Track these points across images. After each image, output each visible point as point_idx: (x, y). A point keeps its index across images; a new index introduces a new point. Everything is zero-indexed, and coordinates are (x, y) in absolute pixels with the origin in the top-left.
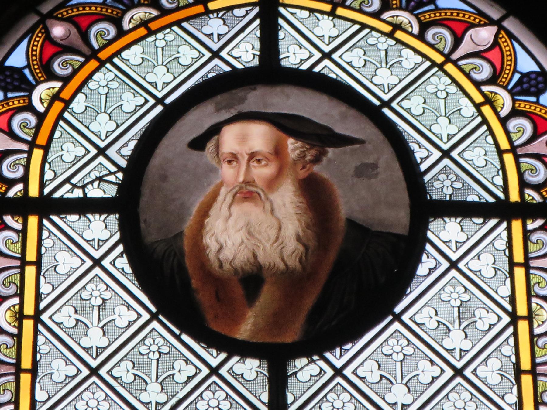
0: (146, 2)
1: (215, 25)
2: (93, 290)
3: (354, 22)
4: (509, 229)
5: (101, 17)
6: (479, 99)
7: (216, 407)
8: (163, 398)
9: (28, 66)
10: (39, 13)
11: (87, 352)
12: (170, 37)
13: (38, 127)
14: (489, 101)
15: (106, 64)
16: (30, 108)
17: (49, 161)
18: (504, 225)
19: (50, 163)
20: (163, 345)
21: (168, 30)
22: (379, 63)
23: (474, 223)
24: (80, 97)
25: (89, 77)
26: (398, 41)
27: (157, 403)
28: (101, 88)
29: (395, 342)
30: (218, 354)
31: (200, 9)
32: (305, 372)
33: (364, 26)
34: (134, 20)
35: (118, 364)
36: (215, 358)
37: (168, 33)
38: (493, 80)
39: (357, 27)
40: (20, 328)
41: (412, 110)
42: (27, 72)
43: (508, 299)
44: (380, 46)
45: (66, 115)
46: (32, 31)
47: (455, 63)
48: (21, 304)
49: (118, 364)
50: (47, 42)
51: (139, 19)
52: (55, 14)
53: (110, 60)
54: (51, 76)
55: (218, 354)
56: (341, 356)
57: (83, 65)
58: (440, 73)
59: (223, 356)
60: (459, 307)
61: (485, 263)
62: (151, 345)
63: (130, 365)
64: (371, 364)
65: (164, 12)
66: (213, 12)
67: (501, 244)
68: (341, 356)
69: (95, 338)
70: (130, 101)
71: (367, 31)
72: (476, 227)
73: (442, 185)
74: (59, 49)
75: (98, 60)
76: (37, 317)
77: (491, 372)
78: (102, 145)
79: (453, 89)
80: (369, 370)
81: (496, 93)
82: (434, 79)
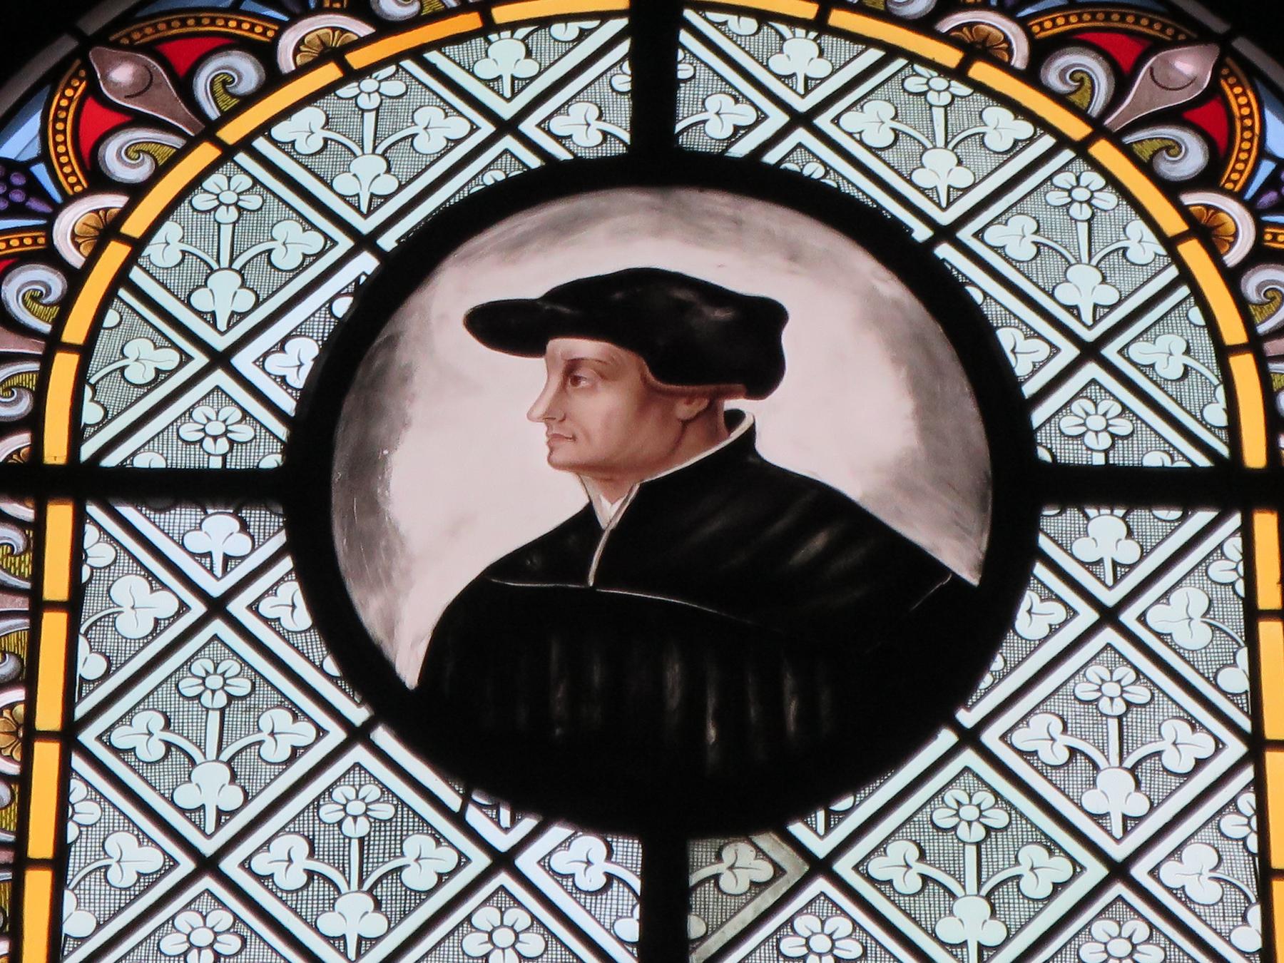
0: (337, 5)
1: (505, 56)
2: (207, 673)
3: (870, 42)
4: (1246, 532)
5: (226, 41)
6: (1173, 224)
7: (1125, 958)
8: (994, 934)
9: (44, 157)
10: (78, 34)
11: (1098, 824)
12: (395, 88)
13: (66, 304)
14: (1205, 231)
15: (236, 154)
16: (50, 257)
17: (93, 381)
18: (1235, 520)
19: (94, 387)
20: (377, 801)
21: (392, 69)
22: (934, 141)
23: (1155, 517)
24: (170, 229)
25: (196, 183)
26: (979, 87)
27: (981, 947)
28: (223, 208)
29: (351, 793)
30: (514, 821)
31: (471, 21)
32: (735, 868)
33: (892, 52)
34: (971, 32)
35: (880, 849)
36: (821, 837)
37: (386, 79)
38: (1208, 179)
39: (874, 55)
40: (27, 762)
41: (1007, 250)
42: (40, 171)
43: (1243, 700)
44: (932, 97)
45: (136, 275)
46: (53, 79)
47: (1115, 139)
48: (30, 703)
49: (880, 849)
50: (90, 104)
51: (318, 42)
52: (113, 38)
53: (245, 145)
54: (100, 181)
55: (514, 821)
56: (828, 828)
57: (179, 155)
58: (1080, 165)
59: (528, 824)
60: (222, 710)
61: (1183, 617)
62: (348, 801)
63: (301, 847)
64: (903, 849)
65: (386, 27)
66: (499, 28)
67: (1226, 570)
68: (828, 828)
69: (210, 787)
70: (293, 242)
71: (901, 62)
72: (1169, 527)
73: (1077, 428)
74: (127, 119)
75: (219, 143)
76: (68, 736)
77: (1195, 873)
78: (220, 343)
79: (1108, 199)
80: (898, 865)
81: (1217, 210)
82: (1065, 179)
